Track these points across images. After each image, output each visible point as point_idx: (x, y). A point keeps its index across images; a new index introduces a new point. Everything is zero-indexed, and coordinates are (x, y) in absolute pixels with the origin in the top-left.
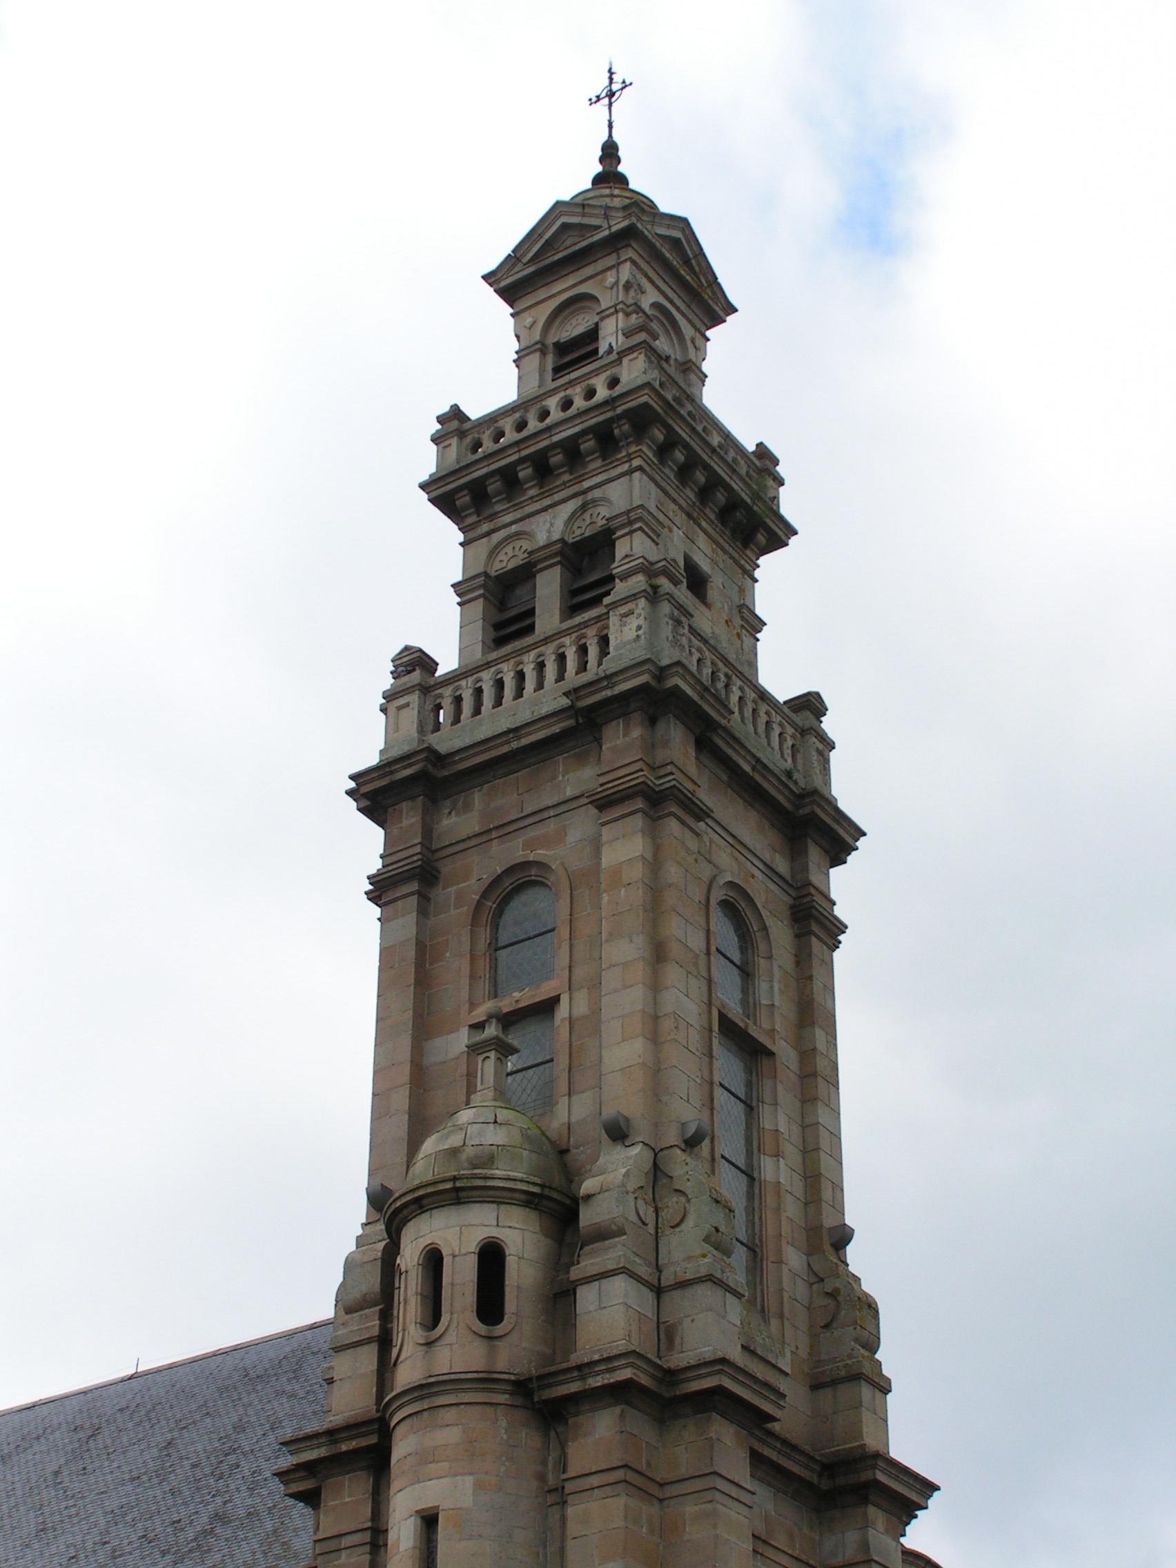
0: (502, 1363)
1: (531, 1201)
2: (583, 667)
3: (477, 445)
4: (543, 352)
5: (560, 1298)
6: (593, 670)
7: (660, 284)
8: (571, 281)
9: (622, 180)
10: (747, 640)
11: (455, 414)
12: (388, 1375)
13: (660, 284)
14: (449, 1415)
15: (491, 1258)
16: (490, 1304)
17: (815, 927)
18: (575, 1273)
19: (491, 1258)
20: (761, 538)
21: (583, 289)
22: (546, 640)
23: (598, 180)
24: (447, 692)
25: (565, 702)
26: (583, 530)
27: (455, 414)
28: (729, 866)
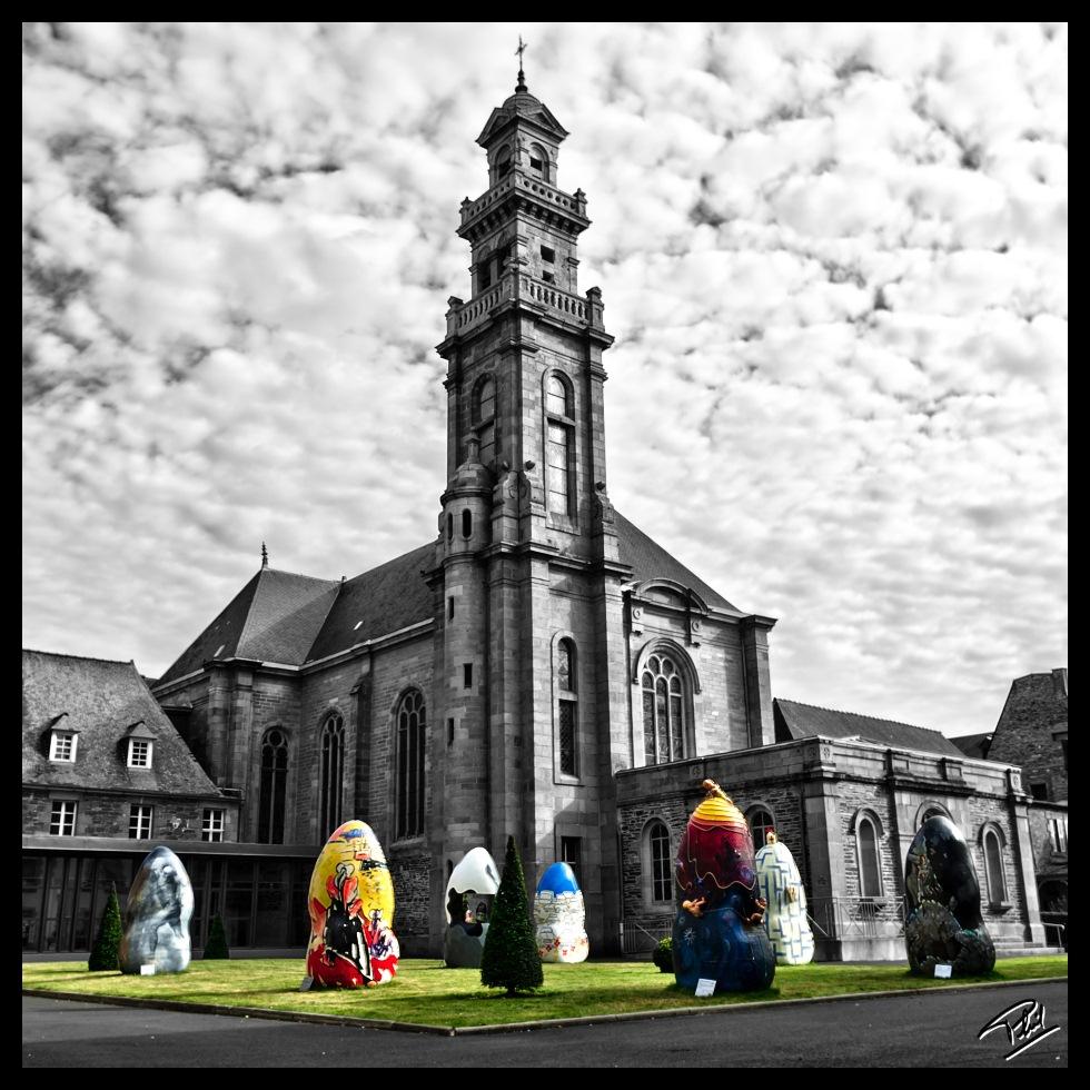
0: (470, 548)
1: (477, 495)
2: (497, 301)
3: (473, 213)
4: (495, 170)
5: (488, 527)
6: (495, 306)
7: (530, 132)
8: (498, 142)
9: (525, 89)
10: (572, 270)
11: (467, 201)
12: (595, 444)
13: (530, 132)
14: (456, 567)
15: (467, 514)
16: (467, 531)
17: (592, 377)
18: (492, 517)
19: (467, 514)
20: (577, 228)
21: (505, 142)
22: (496, 286)
23: (517, 89)
24: (468, 308)
25: (489, 317)
26: (503, 244)
27: (467, 201)
28: (552, 362)
